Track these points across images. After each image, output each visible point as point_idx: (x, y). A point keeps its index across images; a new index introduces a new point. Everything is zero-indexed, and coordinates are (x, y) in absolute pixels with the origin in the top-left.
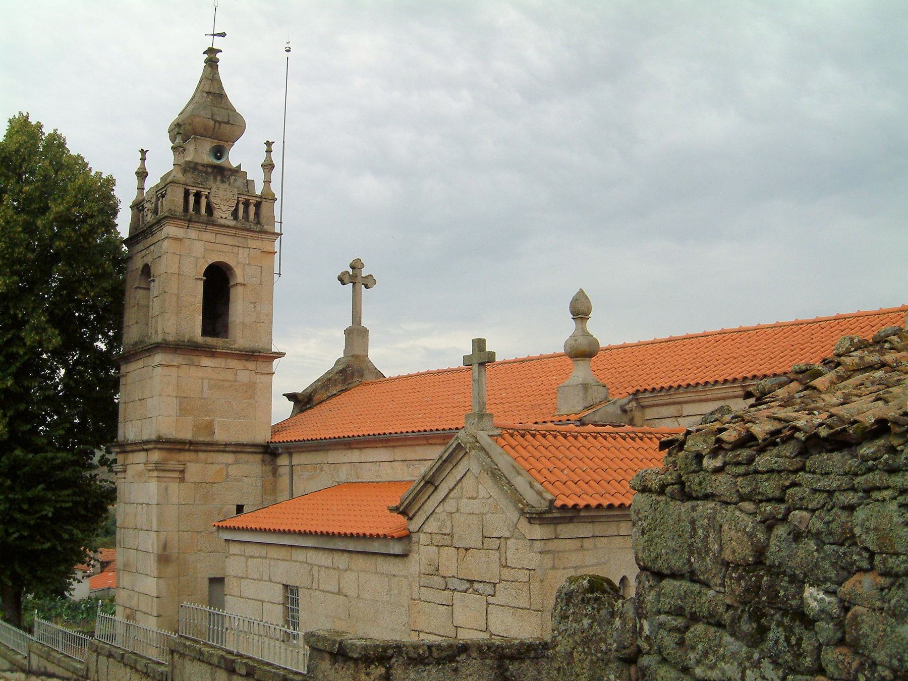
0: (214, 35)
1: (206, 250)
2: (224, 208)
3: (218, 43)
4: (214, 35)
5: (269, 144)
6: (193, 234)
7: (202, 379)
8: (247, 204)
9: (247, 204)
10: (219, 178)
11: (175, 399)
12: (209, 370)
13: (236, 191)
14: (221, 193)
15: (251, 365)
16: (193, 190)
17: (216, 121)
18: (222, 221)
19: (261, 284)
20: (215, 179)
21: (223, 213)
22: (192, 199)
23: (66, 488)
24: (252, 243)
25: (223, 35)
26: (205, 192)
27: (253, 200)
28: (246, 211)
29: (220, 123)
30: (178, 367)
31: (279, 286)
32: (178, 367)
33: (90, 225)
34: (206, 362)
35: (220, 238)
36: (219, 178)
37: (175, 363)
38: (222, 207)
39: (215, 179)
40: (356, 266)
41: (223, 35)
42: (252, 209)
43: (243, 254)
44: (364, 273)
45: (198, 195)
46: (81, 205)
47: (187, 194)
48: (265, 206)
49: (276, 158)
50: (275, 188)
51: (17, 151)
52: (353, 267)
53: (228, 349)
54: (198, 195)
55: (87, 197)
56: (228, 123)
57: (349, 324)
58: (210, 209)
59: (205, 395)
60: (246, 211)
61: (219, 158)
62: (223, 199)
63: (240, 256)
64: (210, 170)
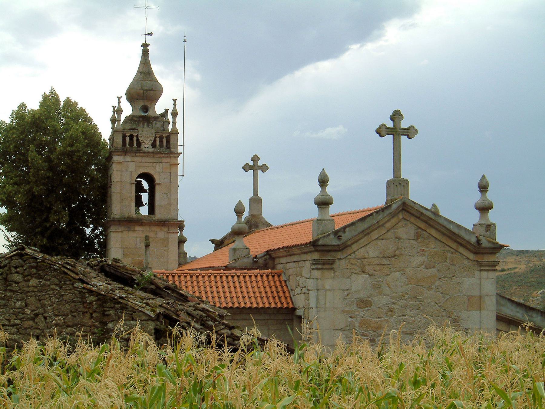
0: (146, 35)
1: (136, 166)
2: (147, 142)
3: (148, 40)
4: (146, 35)
5: (175, 101)
6: (128, 159)
7: (136, 237)
8: (161, 138)
9: (161, 138)
10: (146, 124)
11: (120, 250)
12: (140, 232)
13: (153, 131)
14: (144, 134)
15: (165, 229)
16: (128, 134)
17: (144, 90)
18: (146, 150)
19: (170, 182)
20: (143, 124)
21: (146, 145)
22: (128, 139)
23: (118, 304)
24: (165, 160)
25: (151, 34)
26: (135, 134)
27: (165, 135)
28: (161, 141)
29: (147, 90)
30: (122, 232)
31: (182, 182)
32: (122, 232)
33: (78, 156)
34: (138, 228)
35: (145, 159)
36: (146, 124)
37: (120, 230)
38: (145, 141)
39: (143, 124)
40: (255, 159)
41: (151, 34)
42: (165, 140)
43: (158, 167)
44: (260, 163)
45: (131, 137)
46: (72, 146)
47: (124, 137)
48: (172, 138)
49: (179, 109)
50: (179, 126)
51: (39, 118)
52: (392, 118)
53: (149, 220)
54: (131, 137)
55: (76, 141)
56: (152, 90)
57: (251, 195)
58: (139, 144)
59: (138, 246)
60: (161, 141)
61: (146, 112)
62: (146, 136)
63: (157, 168)
64: (141, 119)
